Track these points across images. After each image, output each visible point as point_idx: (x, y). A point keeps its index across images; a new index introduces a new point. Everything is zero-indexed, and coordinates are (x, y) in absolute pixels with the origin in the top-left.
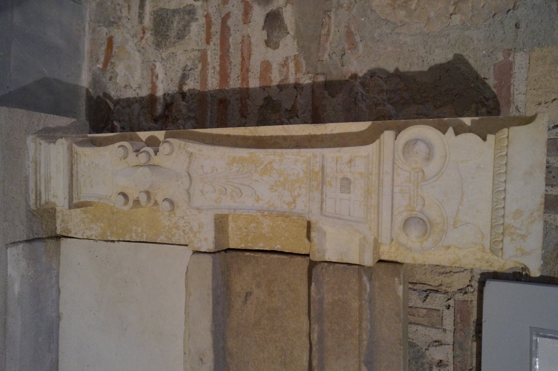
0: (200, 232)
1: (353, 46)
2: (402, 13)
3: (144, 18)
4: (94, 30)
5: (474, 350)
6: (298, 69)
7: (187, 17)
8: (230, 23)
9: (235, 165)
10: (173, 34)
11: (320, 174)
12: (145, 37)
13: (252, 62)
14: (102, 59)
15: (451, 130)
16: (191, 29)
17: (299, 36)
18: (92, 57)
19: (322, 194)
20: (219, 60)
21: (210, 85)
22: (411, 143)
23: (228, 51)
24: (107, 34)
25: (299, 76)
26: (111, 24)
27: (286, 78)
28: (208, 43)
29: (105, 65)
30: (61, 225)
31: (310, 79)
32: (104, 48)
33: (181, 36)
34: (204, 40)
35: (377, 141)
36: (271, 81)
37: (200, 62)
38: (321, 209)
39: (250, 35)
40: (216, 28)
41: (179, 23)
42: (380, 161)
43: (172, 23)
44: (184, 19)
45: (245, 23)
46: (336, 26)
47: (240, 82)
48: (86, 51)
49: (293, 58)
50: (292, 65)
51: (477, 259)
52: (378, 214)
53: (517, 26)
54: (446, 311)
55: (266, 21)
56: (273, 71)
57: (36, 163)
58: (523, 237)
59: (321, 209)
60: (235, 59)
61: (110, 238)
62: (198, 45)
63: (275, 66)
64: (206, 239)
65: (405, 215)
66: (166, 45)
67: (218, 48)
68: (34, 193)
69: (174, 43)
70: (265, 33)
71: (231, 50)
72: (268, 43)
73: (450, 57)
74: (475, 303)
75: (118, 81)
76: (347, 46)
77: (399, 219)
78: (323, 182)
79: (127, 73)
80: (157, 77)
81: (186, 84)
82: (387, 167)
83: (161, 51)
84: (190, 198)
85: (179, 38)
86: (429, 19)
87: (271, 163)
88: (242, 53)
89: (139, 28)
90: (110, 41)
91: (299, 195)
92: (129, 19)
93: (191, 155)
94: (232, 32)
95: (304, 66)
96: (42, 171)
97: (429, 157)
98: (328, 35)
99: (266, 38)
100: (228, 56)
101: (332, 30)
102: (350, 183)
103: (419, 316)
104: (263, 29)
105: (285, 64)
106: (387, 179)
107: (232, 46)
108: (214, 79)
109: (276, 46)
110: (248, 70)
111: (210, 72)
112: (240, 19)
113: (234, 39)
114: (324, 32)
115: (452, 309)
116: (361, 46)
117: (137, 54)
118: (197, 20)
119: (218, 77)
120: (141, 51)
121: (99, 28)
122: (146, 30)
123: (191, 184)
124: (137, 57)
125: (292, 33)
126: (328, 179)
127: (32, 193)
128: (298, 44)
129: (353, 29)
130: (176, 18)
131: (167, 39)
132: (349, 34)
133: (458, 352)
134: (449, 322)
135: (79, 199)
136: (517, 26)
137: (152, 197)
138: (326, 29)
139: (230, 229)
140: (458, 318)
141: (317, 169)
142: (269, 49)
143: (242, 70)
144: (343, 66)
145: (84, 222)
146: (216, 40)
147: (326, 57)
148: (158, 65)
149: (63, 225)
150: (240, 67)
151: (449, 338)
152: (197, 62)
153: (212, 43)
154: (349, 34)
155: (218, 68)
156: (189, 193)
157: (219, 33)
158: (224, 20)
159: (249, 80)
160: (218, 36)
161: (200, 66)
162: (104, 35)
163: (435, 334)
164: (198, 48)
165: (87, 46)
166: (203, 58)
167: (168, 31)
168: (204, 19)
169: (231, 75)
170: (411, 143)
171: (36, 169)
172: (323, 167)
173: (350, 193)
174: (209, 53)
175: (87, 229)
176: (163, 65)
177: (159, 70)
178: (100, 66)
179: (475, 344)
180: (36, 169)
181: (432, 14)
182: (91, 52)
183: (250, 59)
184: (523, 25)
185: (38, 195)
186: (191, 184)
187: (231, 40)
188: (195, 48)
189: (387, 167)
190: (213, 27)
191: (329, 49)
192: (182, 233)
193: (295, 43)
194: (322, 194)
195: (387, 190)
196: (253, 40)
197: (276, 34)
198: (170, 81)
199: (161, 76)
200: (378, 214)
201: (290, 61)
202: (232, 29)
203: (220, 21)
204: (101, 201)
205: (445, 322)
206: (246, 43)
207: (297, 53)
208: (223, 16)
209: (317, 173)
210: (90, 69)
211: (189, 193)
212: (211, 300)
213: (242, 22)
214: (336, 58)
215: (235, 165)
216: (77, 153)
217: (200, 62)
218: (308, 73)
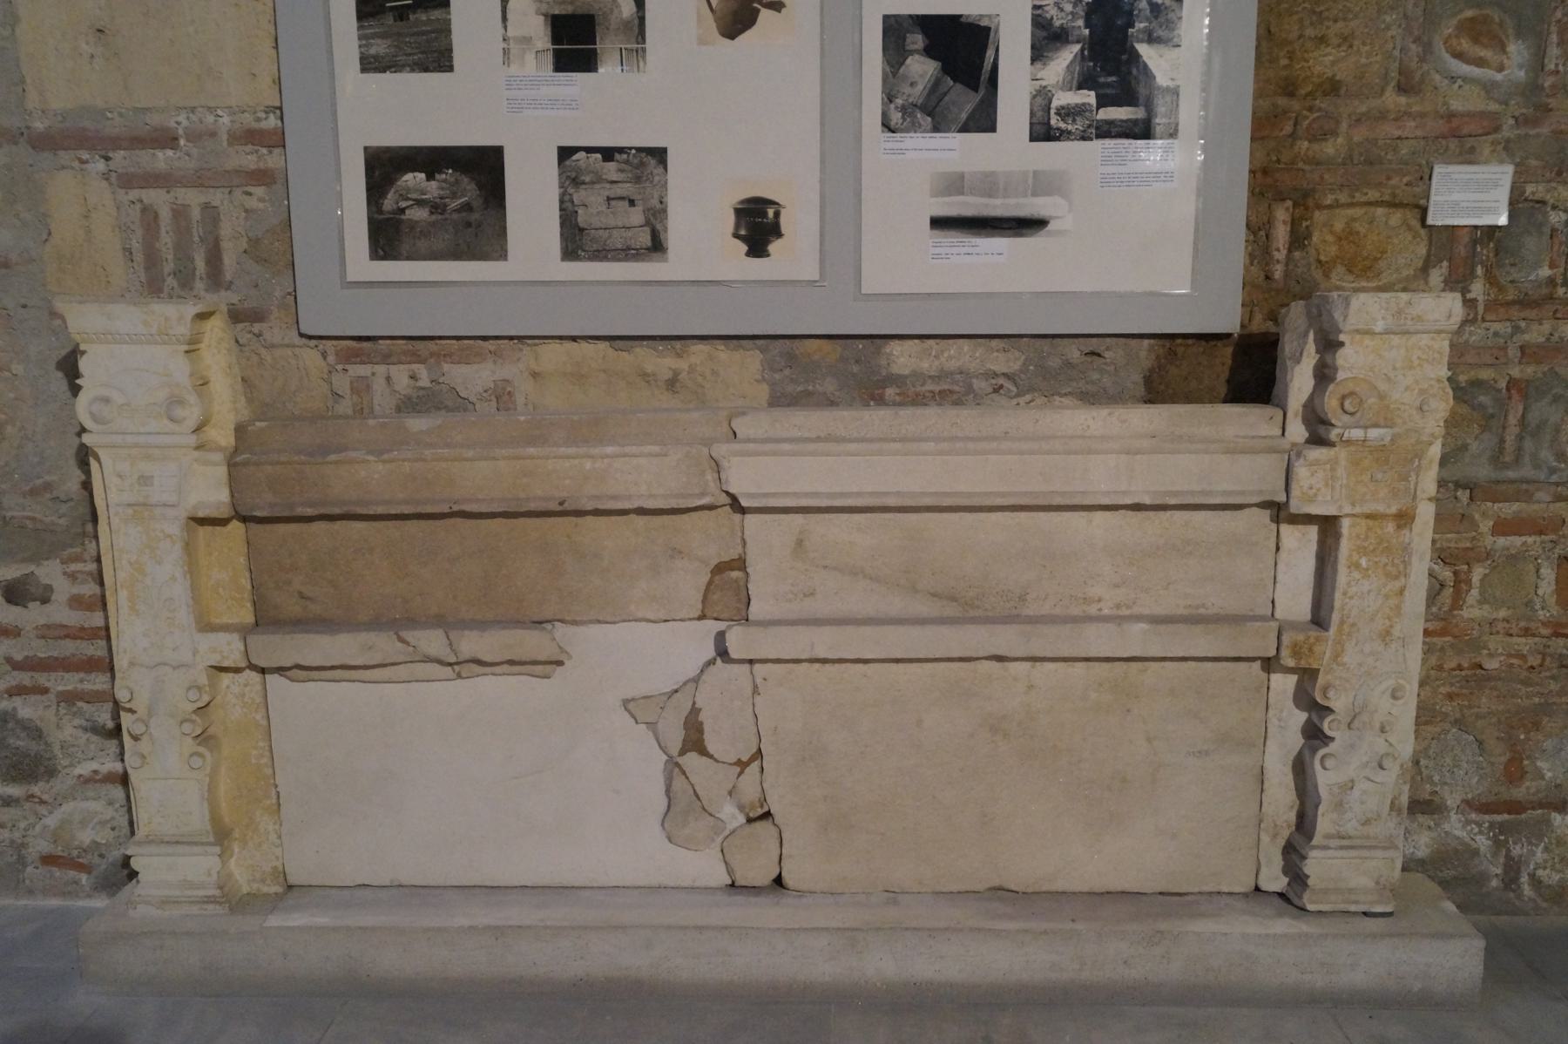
0: (221, 652)
1: (48, 487)
2: (9, 429)
3: (10, 797)
4: (31, 892)
5: (388, 342)
6: (78, 559)
7: (10, 725)
8: (18, 657)
9: (137, 607)
10: (34, 747)
11: (136, 508)
12: (39, 794)
13: (72, 623)
14: (72, 874)
15: (78, 381)
16: (27, 716)
17: (36, 558)
18: (69, 893)
19: (156, 506)
20: (70, 674)
21: (105, 686)
22: (95, 418)
23: (56, 659)
24: (37, 868)
25: (87, 557)
26: (22, 861)
27: (90, 574)
28: (45, 691)
29: (81, 867)
30: (269, 885)
31: (91, 542)
32: (57, 872)
33: (36, 733)
34: (44, 698)
35: (95, 449)
36: (94, 595)
37: (74, 704)
38: (173, 506)
39: (34, 625)
40: (25, 678)
41: (18, 738)
42: (114, 447)
43: (18, 748)
44: (13, 730)
45: (19, 635)
46: (24, 509)
47: (99, 641)
48: (62, 903)
49: (65, 566)
50: (73, 567)
51: (219, 352)
52: (169, 447)
53: (24, 306)
54: (351, 372)
55: (17, 604)
56: (82, 592)
57: (163, 902)
58: (167, 319)
59: (173, 506)
60: (69, 648)
61: (274, 801)
62: (50, 706)
63: (75, 590)
64: (229, 644)
65: (166, 421)
66: (50, 759)
67: (53, 675)
68: (205, 906)
69: (46, 743)
70: (31, 605)
71: (55, 654)
72: (45, 601)
73: (60, 375)
74: (334, 342)
75: (104, 842)
76: (48, 496)
77: (171, 426)
78: (145, 505)
79: (91, 826)
80: (95, 772)
81: (105, 724)
82: (118, 439)
83: (59, 768)
84: (183, 665)
85: (40, 737)
86: (16, 399)
87: (131, 564)
88: (60, 638)
89: (27, 805)
90: (49, 860)
91: (162, 531)
92: (14, 826)
93: (132, 664)
94: (31, 654)
95: (74, 550)
96: (177, 893)
97: (107, 400)
98: (33, 519)
99: (38, 603)
100: (63, 659)
101: (29, 514)
102: (142, 476)
103: (362, 403)
104: (26, 607)
105: (72, 576)
106: (130, 439)
107: (50, 654)
108: (97, 681)
109: (49, 588)
110: (82, 629)
111: (87, 686)
112: (14, 641)
113: (43, 651)
114: (29, 524)
115: (347, 367)
116: (48, 478)
117: (64, 808)
118: (15, 709)
119: (93, 675)
120: (56, 803)
121: (27, 882)
122: (30, 793)
123: (165, 664)
124: (68, 807)
125: (32, 568)
126: (141, 500)
127: (206, 910)
128: (47, 559)
129: (28, 488)
130: (11, 741)
131: (42, 756)
132: (34, 492)
133: (394, 359)
134: (362, 370)
135: (208, 832)
136: (24, 306)
137: (188, 717)
138: (28, 522)
139: (230, 621)
140: (1284, 222)
141: (130, 511)
142: (53, 598)
143: (82, 638)
144: (72, 499)
145: (260, 845)
146: (42, 679)
147: (62, 521)
148: (78, 771)
149: (268, 882)
150: (79, 641)
151: (381, 369)
152: (75, 709)
153: (47, 684)
154: (34, 492)
155: (82, 675)
156: (178, 667)
157: (33, 674)
158: (17, 666)
159: (93, 626)
160: (36, 675)
161: (80, 704)
162: (38, 871)
163: (379, 385)
164: (54, 707)
165: (54, 902)
166: (69, 698)
167: (30, 755)
168: (14, 698)
169: (89, 654)
170: (95, 418)
171: (174, 902)
172: (129, 505)
173: (152, 477)
174: (60, 688)
175: (268, 839)
176: (79, 762)
177: (85, 769)
178: (84, 878)
179: (380, 342)
180: (174, 902)
181: (12, 395)
182: (64, 894)
183: (66, 626)
184: (23, 301)
185: (210, 900)
186: (165, 664)
187: (43, 655)
188: (54, 711)
189: (118, 439)
190: (24, 683)
191: (53, 518)
192: (248, 688)
193: (46, 563)
194: (156, 506)
195: (142, 439)
196: (42, 622)
197: (33, 590)
198: (103, 753)
199: (94, 766)
200: (169, 447)
201: (68, 570)
202: (26, 654)
203: (15, 673)
204: (206, 796)
205: (363, 374)
206: (50, 632)
207: (58, 560)
208: (9, 668)
209: (135, 511)
210: (89, 896)
211: (178, 667)
212: (300, 636)
213: (18, 639)
214: (64, 508)
215: (137, 607)
216: (147, 836)
217: (74, 704)
218: (83, 544)
